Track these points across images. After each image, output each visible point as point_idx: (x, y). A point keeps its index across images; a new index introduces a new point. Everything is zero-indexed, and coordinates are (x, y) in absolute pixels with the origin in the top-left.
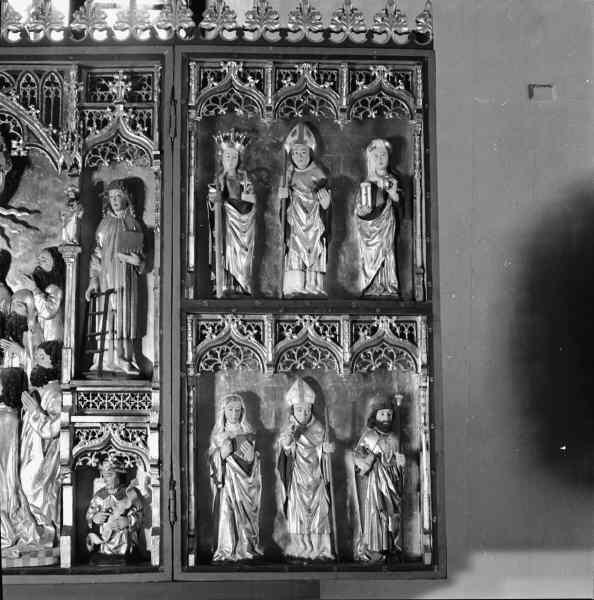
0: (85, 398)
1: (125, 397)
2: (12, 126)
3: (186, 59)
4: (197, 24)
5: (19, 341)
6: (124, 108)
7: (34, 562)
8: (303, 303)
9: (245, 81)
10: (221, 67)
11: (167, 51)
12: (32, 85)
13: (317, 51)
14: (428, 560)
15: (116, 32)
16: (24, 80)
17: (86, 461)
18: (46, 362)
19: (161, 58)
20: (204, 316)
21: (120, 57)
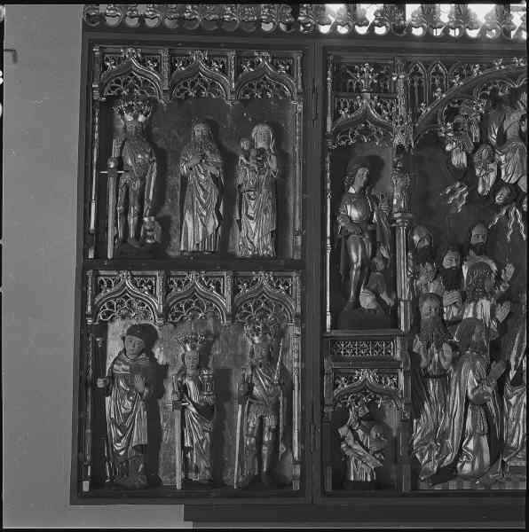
4: (296, 18)
8: (258, 262)
9: (277, 68)
10: (121, 53)
12: (420, 75)
13: (173, 38)
14: (296, 486)
16: (433, 70)
20: (102, 272)
21: (439, 51)
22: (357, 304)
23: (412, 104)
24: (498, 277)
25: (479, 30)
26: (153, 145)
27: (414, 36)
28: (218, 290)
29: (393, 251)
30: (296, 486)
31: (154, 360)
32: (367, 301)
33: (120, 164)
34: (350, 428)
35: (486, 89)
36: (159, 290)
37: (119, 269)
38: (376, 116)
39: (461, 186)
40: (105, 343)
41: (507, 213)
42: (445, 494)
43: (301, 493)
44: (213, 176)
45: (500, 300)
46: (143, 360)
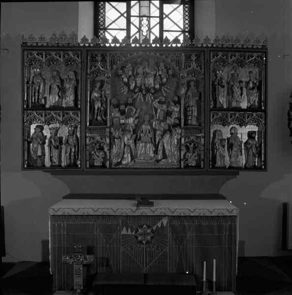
3: (210, 51)
5: (170, 117)
7: (175, 167)
11: (206, 50)
14: (263, 167)
18: (177, 122)
19: (81, 50)
22: (97, 119)
23: (112, 65)
24: (136, 112)
26: (42, 77)
27: (106, 46)
28: (77, 116)
29: (106, 105)
30: (79, 166)
31: (43, 134)
32: (99, 118)
33: (33, 83)
34: (95, 152)
36: (79, 115)
37: (33, 110)
38: (102, 69)
40: (30, 130)
42: (119, 168)
43: (80, 168)
44: (57, 85)
45: (136, 118)
46: (40, 134)
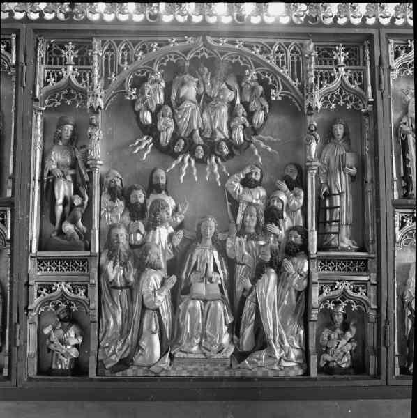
0: (323, 264)
1: (349, 263)
2: (271, 80)
6: (345, 70)
11: (23, 26)
12: (297, 52)
15: (193, 16)
17: (327, 306)
25: (389, 19)
35: (163, 61)
39: (148, 139)
41: (183, 160)
42: (125, 380)
